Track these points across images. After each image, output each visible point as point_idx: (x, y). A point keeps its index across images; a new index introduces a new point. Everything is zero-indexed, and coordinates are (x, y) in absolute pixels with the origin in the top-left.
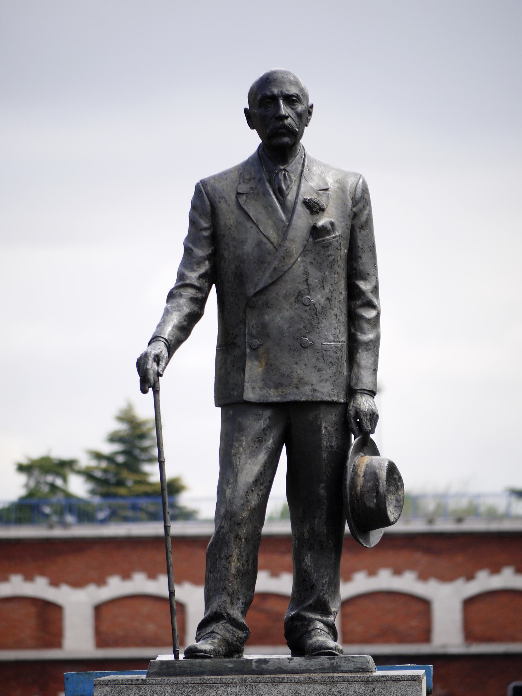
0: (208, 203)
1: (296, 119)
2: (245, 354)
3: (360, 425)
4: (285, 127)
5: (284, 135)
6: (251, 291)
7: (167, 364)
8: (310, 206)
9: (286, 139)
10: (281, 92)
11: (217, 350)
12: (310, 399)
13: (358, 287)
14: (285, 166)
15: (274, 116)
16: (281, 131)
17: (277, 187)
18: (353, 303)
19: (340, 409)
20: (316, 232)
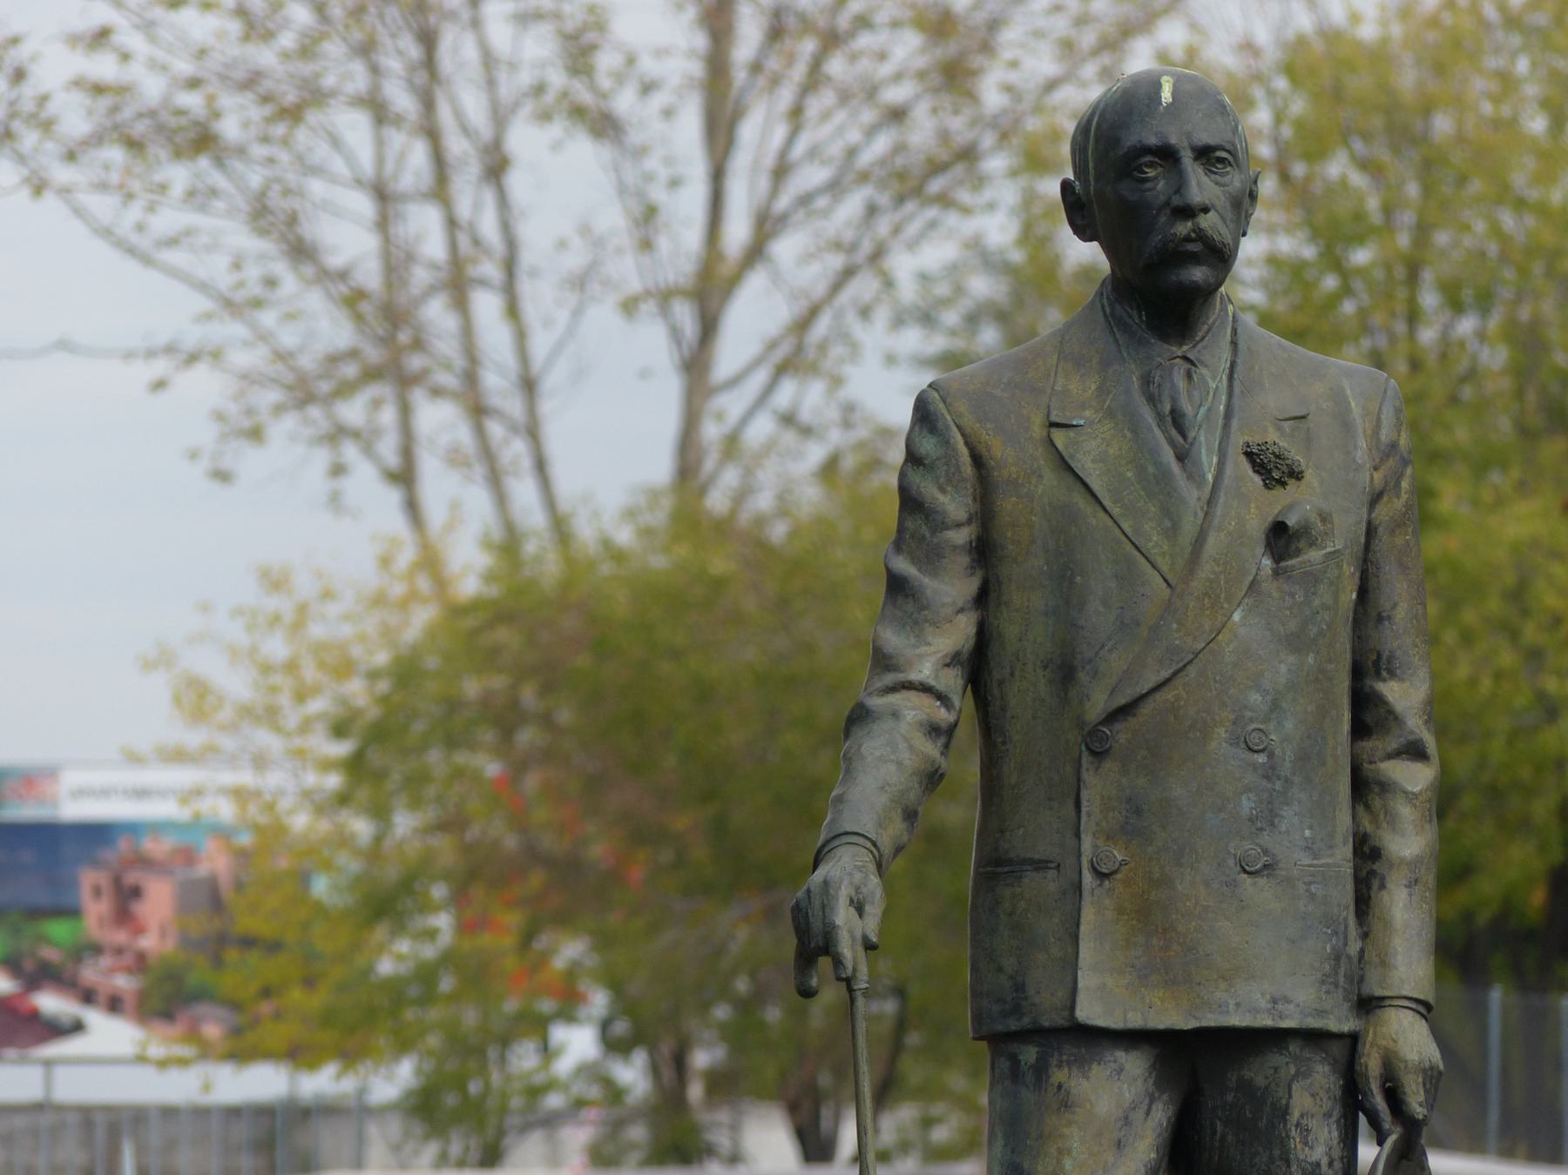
0: (964, 451)
1: (1229, 215)
2: (1078, 887)
3: (1394, 1096)
4: (1201, 236)
5: (1194, 259)
6: (1098, 703)
7: (105, 232)
8: (1262, 465)
9: (1198, 274)
10: (1189, 136)
11: (1507, 1153)
12: (1268, 1022)
13: (1380, 700)
14: (1185, 348)
15: (1167, 203)
16: (1191, 247)
17: (1168, 408)
18: (1367, 745)
19: (1338, 1049)
20: (1281, 538)
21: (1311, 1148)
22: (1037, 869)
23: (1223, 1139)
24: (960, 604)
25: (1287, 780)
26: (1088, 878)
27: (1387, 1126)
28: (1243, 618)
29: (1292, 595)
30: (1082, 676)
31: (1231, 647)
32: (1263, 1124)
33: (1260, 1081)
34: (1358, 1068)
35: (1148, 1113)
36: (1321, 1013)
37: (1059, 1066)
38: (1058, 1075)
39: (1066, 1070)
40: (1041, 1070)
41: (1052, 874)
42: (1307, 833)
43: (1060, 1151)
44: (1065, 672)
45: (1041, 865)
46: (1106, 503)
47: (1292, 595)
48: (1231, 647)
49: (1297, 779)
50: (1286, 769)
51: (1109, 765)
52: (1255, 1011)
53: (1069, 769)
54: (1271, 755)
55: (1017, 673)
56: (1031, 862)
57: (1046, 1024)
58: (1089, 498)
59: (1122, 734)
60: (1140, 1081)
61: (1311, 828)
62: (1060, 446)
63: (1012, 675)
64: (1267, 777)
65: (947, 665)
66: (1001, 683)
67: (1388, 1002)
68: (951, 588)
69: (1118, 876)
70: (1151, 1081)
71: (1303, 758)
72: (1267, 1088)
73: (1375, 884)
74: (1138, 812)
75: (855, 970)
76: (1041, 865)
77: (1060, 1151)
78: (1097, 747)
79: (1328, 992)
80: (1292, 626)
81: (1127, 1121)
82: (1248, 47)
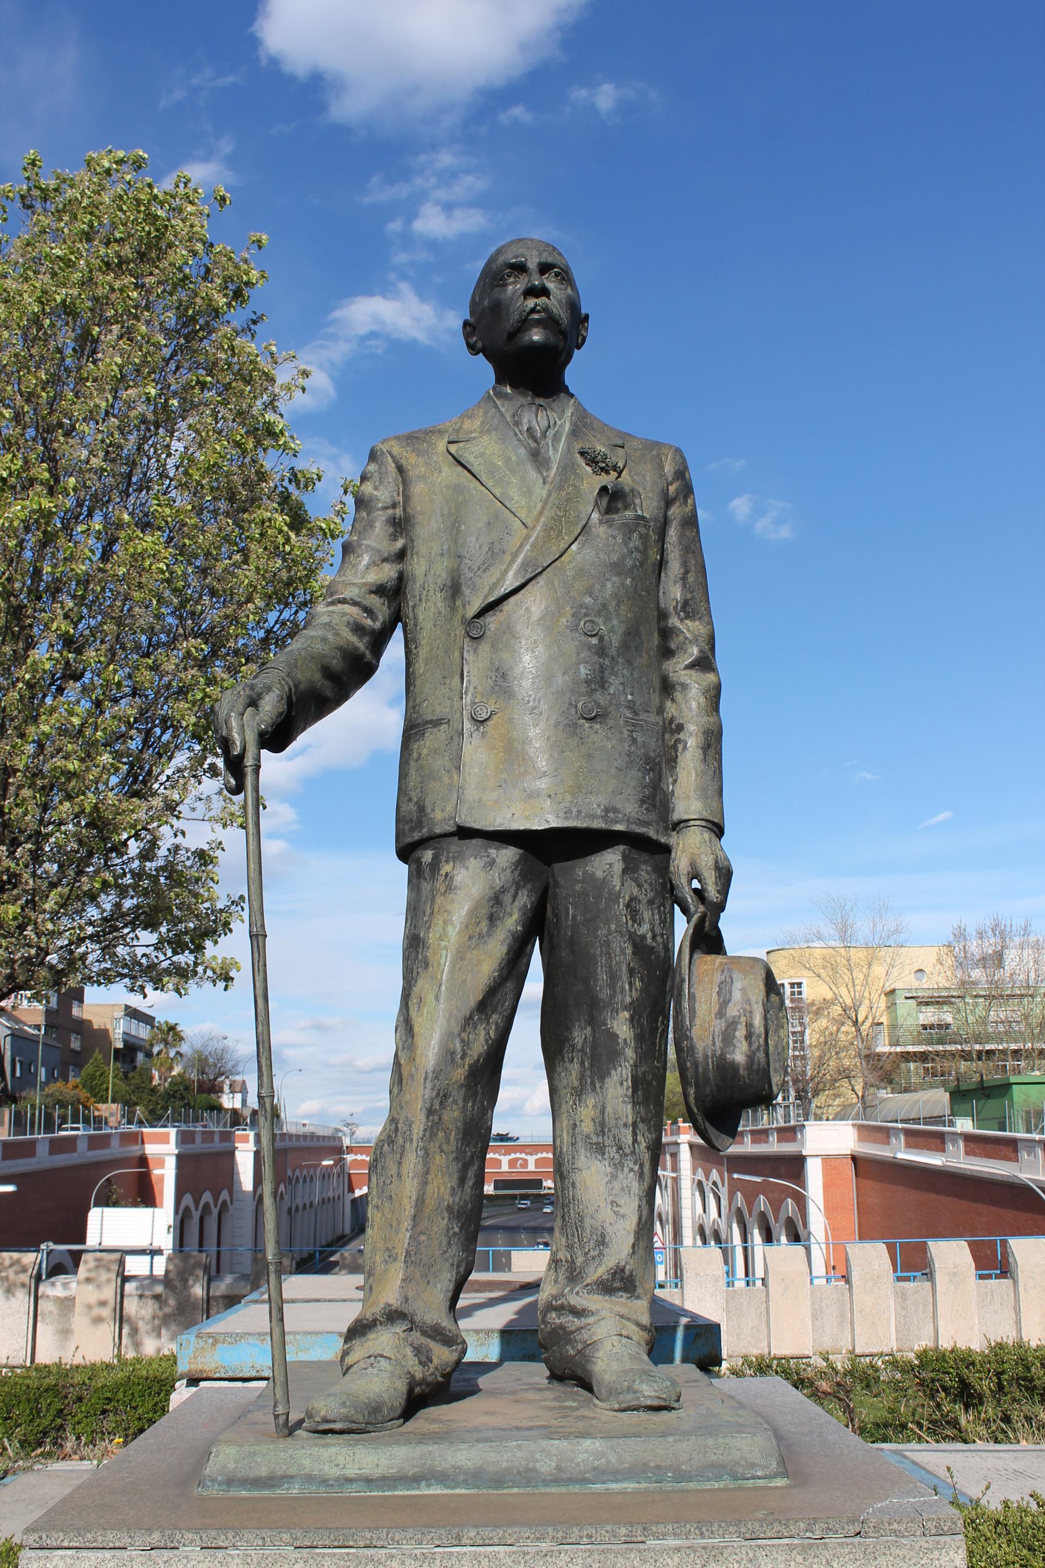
21: (640, 924)
22: (435, 726)
23: (574, 917)
24: (386, 555)
25: (613, 658)
26: (467, 725)
27: (692, 908)
28: (579, 549)
29: (615, 537)
30: (466, 590)
31: (571, 566)
32: (602, 906)
33: (600, 874)
34: (672, 869)
35: (515, 896)
36: (646, 824)
37: (447, 862)
38: (447, 868)
39: (451, 863)
40: (435, 866)
41: (444, 727)
42: (630, 697)
43: (445, 922)
44: (454, 590)
45: (437, 723)
46: (484, 479)
47: (615, 537)
48: (571, 566)
49: (620, 660)
50: (613, 652)
51: (485, 646)
52: (593, 817)
53: (457, 654)
54: (601, 639)
55: (424, 598)
56: (431, 722)
57: (438, 831)
58: (529, 587)
59: (492, 621)
60: (509, 871)
61: (632, 694)
62: (453, 452)
63: (420, 600)
64: (600, 656)
65: (372, 592)
66: (414, 607)
67: (692, 823)
68: (378, 537)
69: (490, 723)
70: (517, 873)
71: (625, 646)
72: (604, 879)
73: (680, 747)
74: (504, 676)
75: (244, 749)
76: (437, 723)
77: (445, 922)
78: (474, 633)
79: (647, 809)
80: (615, 557)
81: (903, 1308)
82: (1006, 1504)
